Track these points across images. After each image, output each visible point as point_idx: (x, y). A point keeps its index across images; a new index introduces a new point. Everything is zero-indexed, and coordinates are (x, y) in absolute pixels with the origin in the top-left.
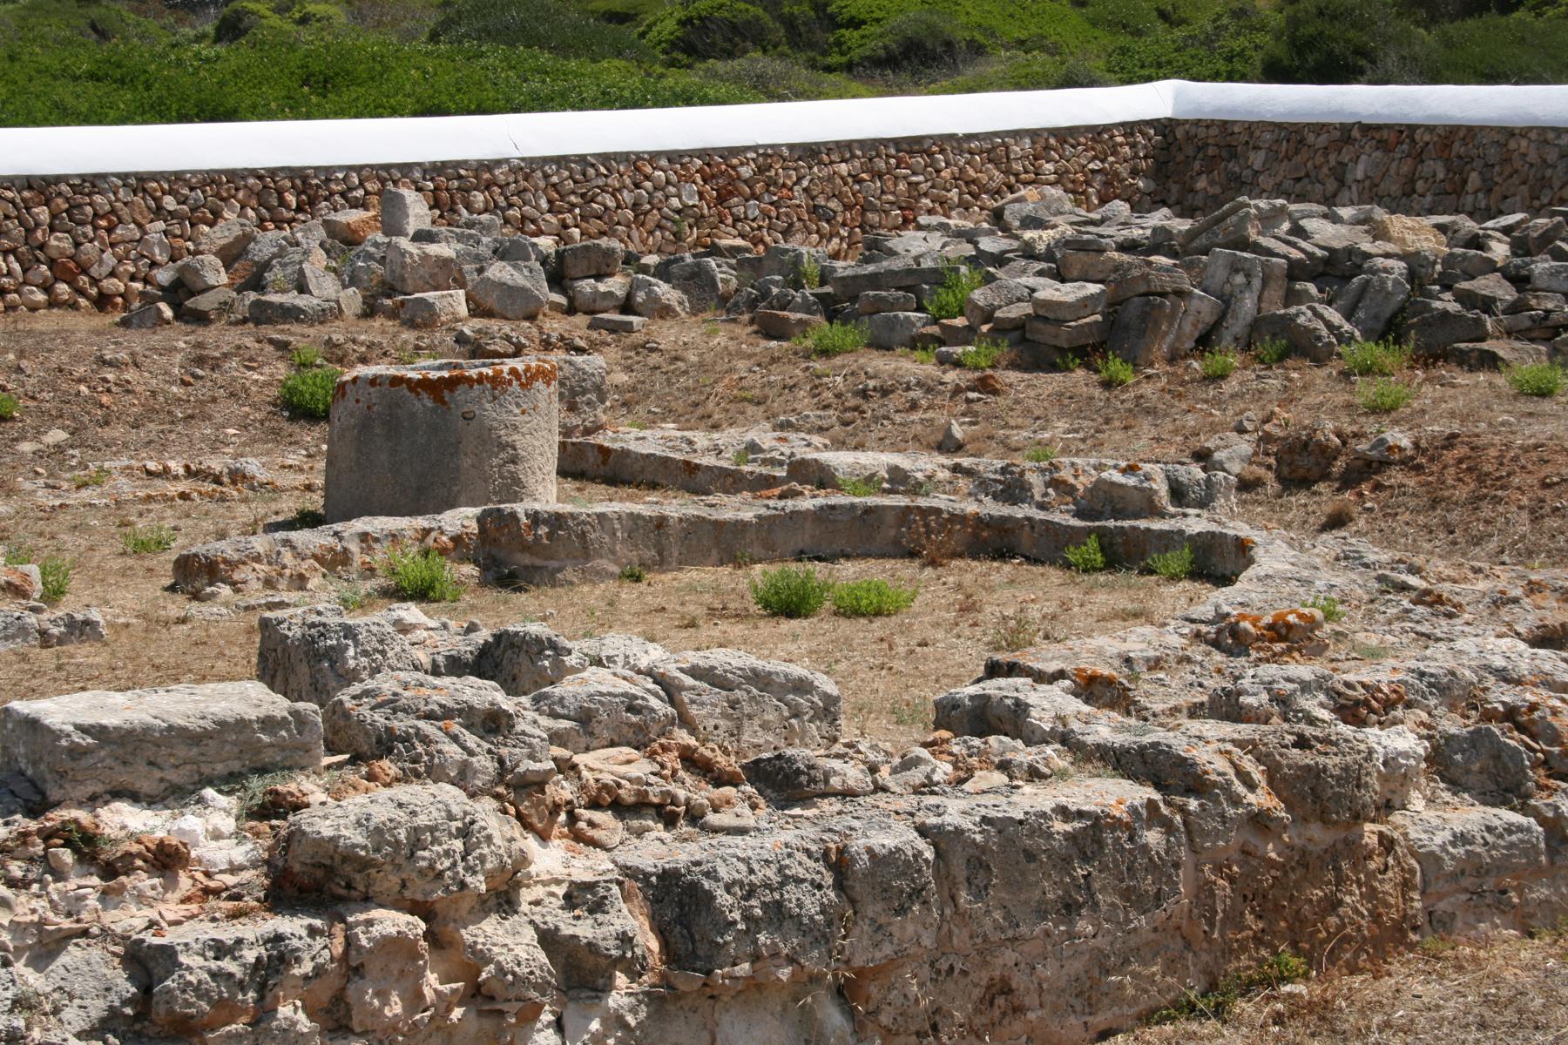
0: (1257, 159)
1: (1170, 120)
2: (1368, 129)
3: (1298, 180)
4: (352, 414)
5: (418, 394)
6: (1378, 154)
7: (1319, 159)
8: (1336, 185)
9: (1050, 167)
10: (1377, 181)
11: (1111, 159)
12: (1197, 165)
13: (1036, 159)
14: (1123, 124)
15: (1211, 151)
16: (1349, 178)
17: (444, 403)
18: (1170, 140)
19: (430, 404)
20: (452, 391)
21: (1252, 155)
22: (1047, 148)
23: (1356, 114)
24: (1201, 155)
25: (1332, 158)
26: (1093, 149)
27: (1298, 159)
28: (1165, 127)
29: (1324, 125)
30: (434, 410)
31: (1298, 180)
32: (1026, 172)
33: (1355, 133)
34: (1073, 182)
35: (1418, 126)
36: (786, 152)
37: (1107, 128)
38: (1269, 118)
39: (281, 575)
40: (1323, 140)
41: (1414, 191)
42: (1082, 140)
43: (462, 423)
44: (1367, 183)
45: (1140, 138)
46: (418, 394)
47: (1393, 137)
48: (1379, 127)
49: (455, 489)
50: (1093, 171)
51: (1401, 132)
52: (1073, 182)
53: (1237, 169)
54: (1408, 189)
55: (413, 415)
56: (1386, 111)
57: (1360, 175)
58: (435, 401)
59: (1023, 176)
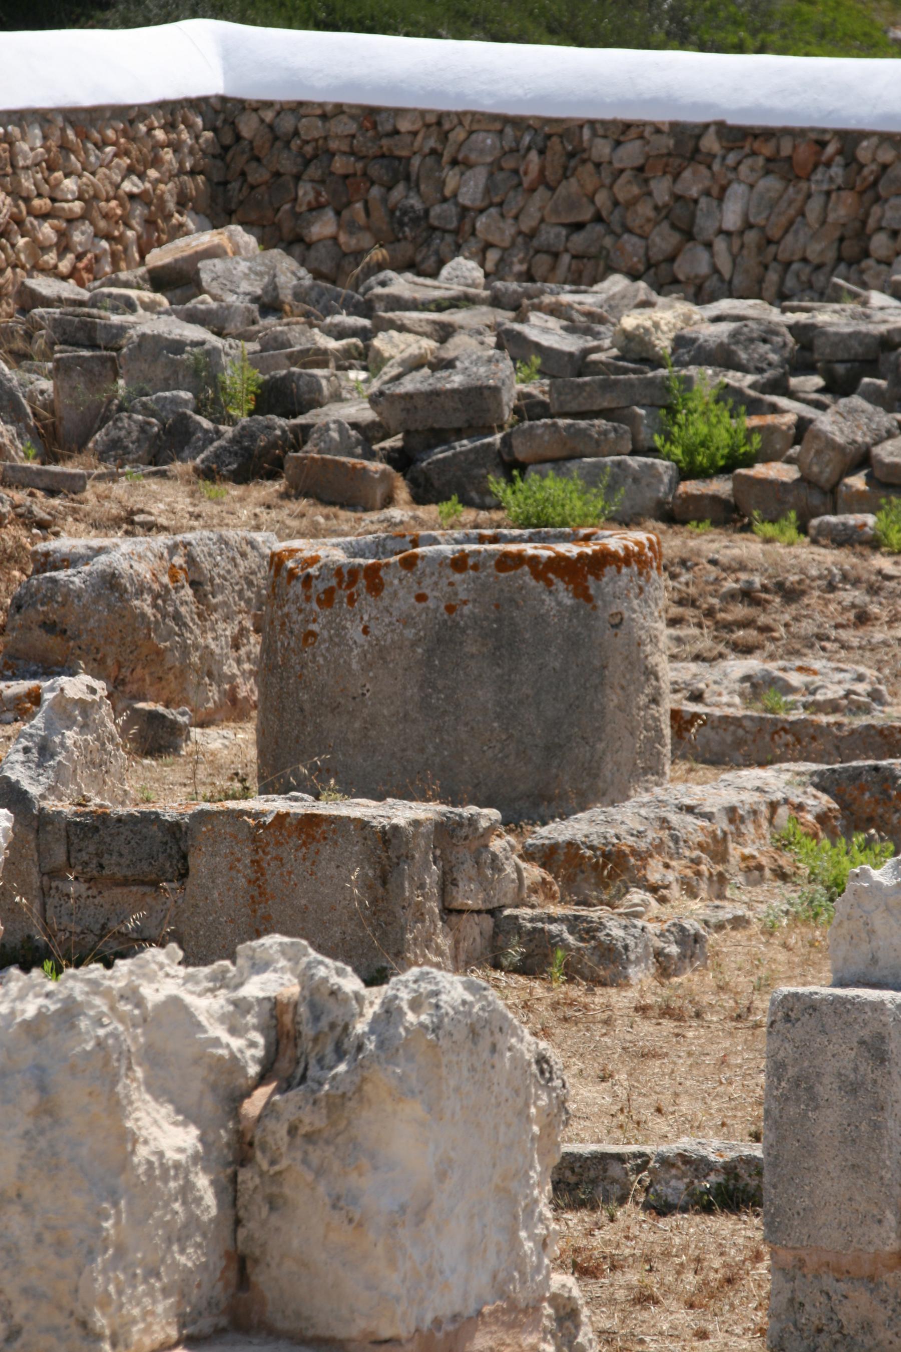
0: (470, 188)
1: (223, 99)
2: (739, 137)
3: (578, 227)
4: (407, 621)
5: (549, 583)
6: (771, 184)
7: (626, 189)
8: (675, 238)
9: (70, 185)
10: (774, 232)
11: (153, 173)
12: (306, 192)
13: (51, 169)
14: (162, 105)
15: (339, 165)
16: (705, 226)
17: (589, 599)
18: (228, 139)
19: (568, 600)
20: (598, 577)
21: (451, 178)
22: (65, 147)
23: (709, 106)
24: (314, 171)
25: (661, 189)
26: (127, 153)
27: (571, 186)
28: (221, 112)
29: (627, 126)
30: (574, 610)
31: (578, 227)
32: (40, 195)
33: (710, 143)
34: (106, 216)
35: (862, 135)
36: (710, 143)
37: (142, 112)
38: (488, 105)
39: (698, 874)
40: (631, 153)
41: (866, 254)
42: (110, 133)
43: (609, 632)
44: (751, 237)
45: (185, 136)
46: (549, 583)
47: (804, 153)
48: (768, 134)
49: (600, 746)
50: (132, 196)
51: (823, 144)
52: (106, 216)
53: (414, 202)
54: (850, 248)
55: (540, 620)
56: (778, 103)
57: (731, 218)
58: (576, 596)
59: (36, 202)
